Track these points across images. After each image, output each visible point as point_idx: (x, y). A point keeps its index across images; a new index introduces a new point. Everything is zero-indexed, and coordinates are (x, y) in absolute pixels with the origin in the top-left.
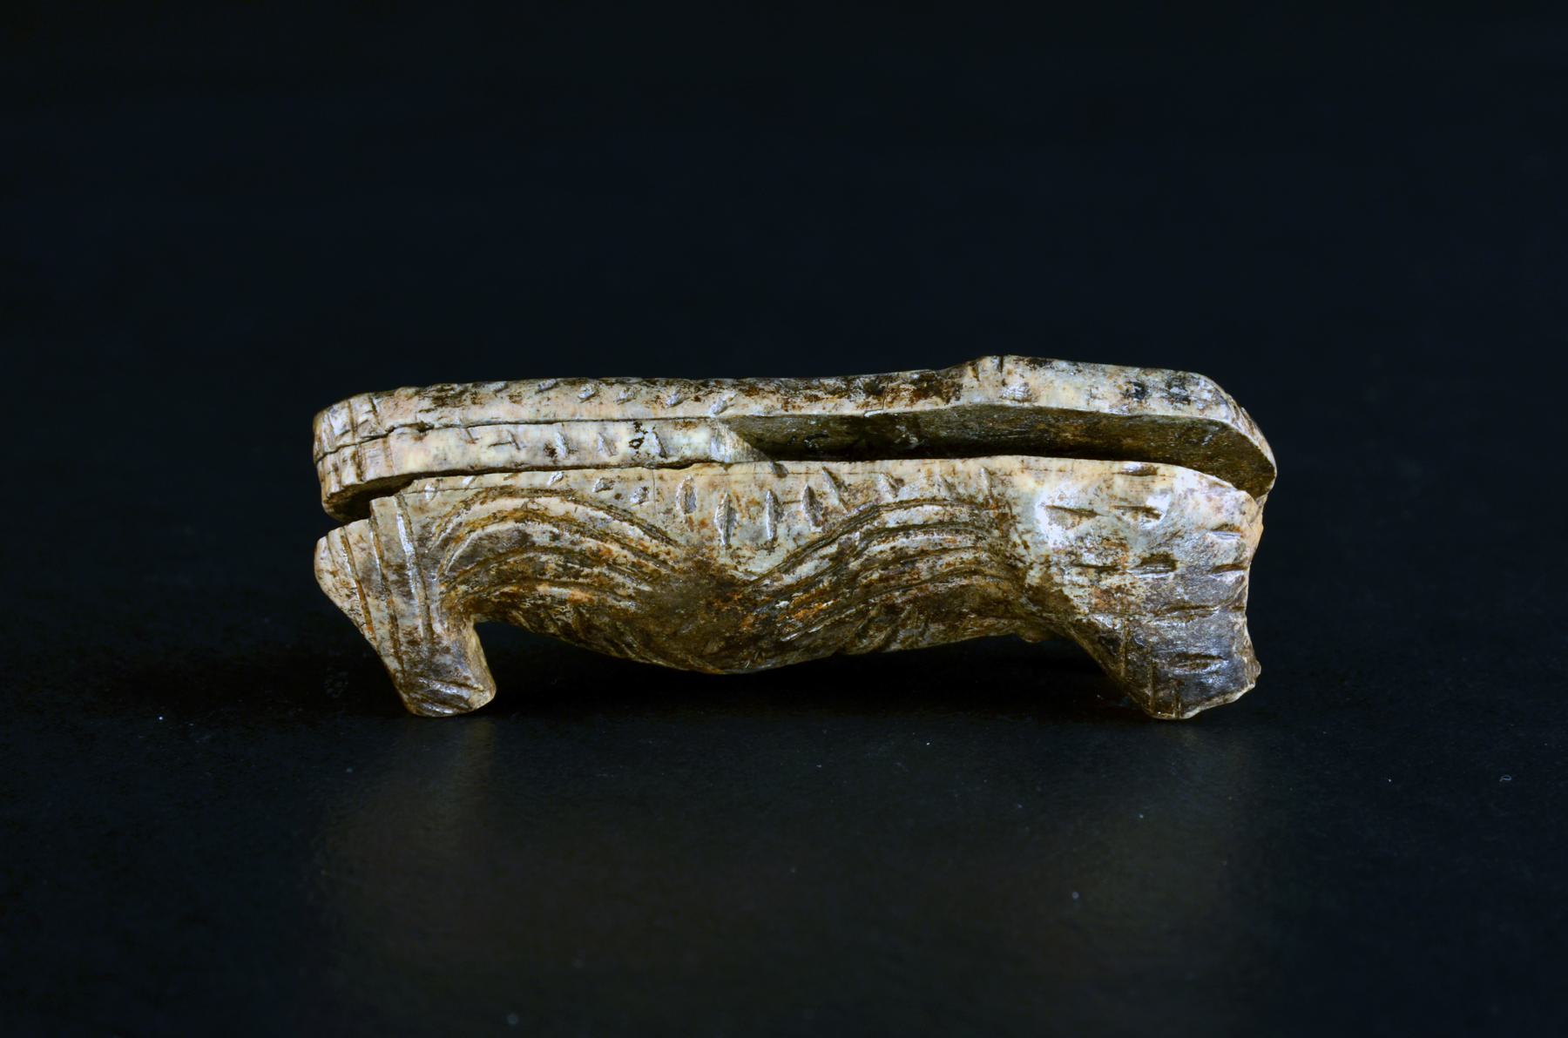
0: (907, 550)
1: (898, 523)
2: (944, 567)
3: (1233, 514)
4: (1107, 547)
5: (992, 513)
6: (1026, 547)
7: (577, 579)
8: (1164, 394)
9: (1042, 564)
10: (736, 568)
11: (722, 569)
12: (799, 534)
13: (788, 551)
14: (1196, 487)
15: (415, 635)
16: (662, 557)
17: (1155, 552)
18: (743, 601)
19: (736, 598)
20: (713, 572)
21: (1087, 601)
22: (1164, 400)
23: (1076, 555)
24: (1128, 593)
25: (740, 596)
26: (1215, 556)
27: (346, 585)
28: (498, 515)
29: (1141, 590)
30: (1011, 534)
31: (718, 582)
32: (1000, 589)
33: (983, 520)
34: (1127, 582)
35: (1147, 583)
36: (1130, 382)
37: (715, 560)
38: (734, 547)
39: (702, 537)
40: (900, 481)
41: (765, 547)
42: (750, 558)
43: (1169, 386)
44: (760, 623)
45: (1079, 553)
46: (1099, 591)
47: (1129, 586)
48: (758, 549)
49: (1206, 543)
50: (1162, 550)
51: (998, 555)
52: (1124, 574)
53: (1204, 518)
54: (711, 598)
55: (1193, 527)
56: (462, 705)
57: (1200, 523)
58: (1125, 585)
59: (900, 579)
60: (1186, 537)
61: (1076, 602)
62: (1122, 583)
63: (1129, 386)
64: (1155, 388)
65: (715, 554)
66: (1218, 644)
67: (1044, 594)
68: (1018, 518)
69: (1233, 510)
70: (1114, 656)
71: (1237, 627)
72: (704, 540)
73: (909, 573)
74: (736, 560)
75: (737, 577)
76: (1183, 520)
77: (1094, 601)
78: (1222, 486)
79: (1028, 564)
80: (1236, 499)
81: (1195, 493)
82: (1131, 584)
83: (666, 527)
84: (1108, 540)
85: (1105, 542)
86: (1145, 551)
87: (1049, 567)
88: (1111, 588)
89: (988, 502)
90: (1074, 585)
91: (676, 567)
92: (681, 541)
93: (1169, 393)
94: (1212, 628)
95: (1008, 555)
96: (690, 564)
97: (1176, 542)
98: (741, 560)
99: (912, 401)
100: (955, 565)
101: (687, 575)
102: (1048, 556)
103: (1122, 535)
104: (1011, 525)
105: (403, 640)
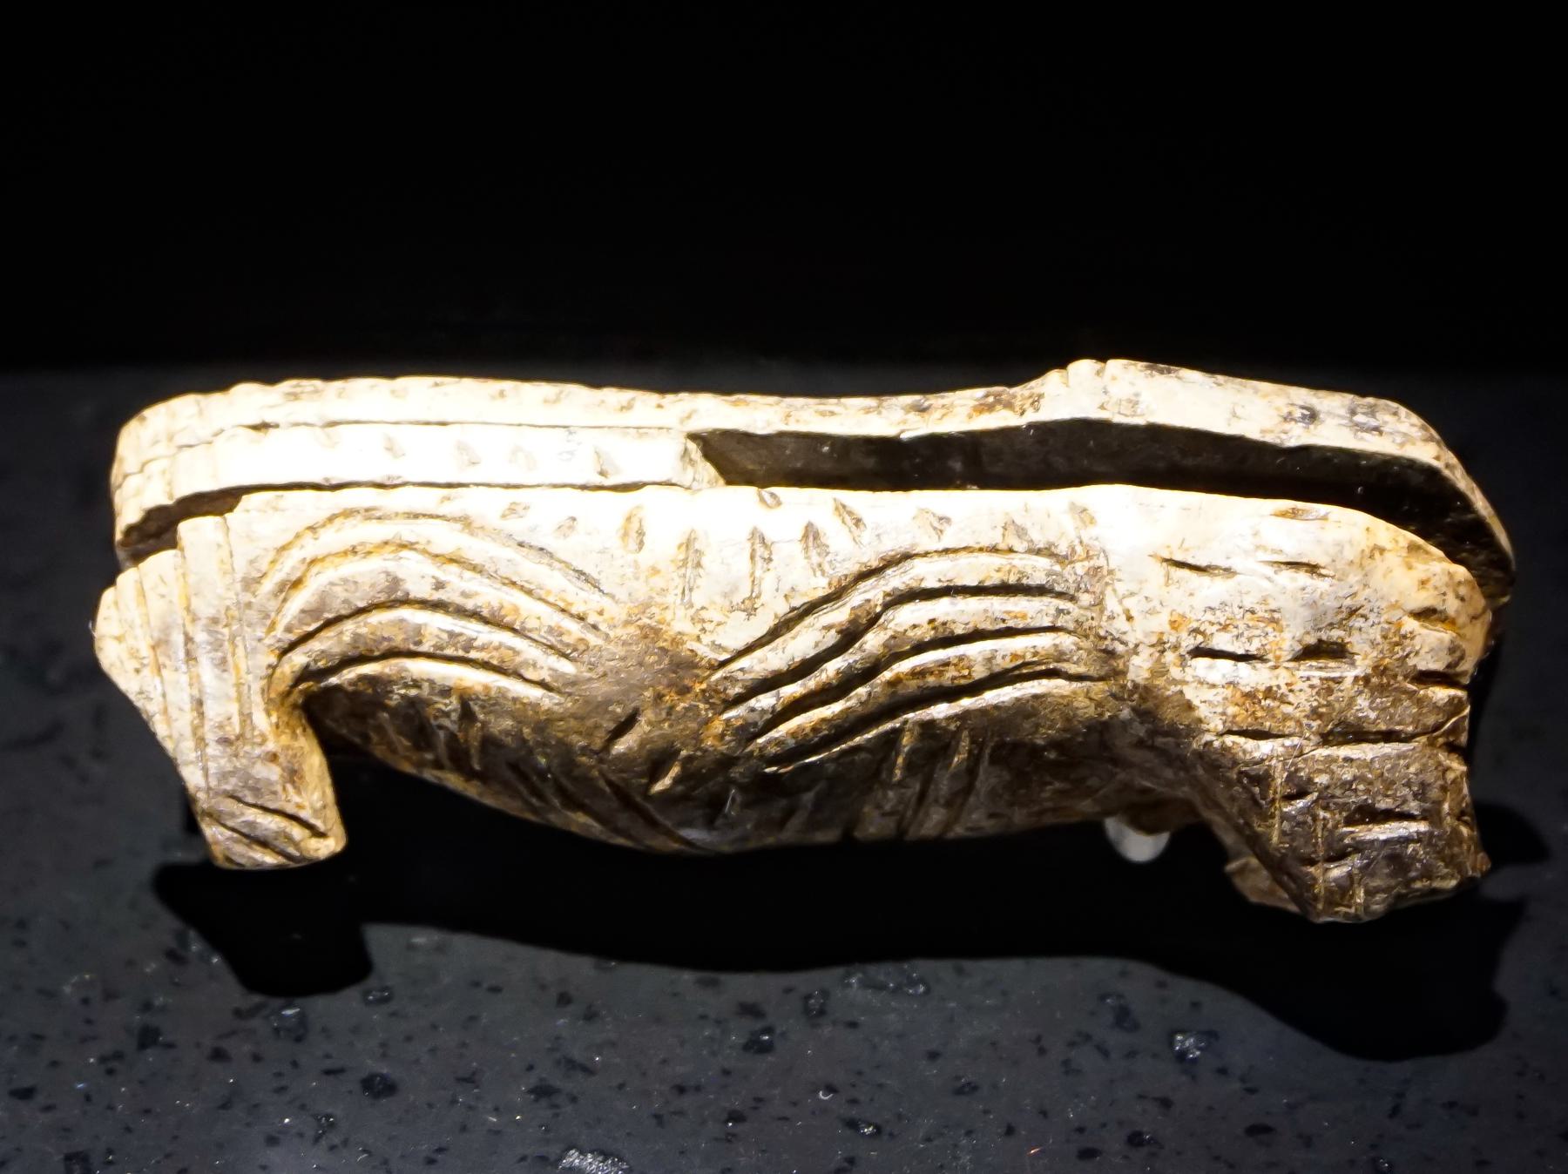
0: (953, 626)
1: (940, 581)
2: (1008, 659)
3: (1444, 594)
4: (1251, 624)
5: (1080, 568)
6: (1130, 618)
7: (468, 652)
8: (1344, 422)
9: (1153, 646)
10: (698, 639)
11: (677, 641)
12: (793, 589)
13: (776, 616)
14: (1388, 546)
15: (228, 728)
16: (591, 619)
17: (1324, 638)
18: (707, 694)
19: (698, 688)
20: (664, 644)
21: (1220, 710)
22: (1344, 428)
23: (1203, 633)
24: (1283, 700)
25: (704, 686)
26: (1417, 653)
27: (134, 654)
28: (358, 548)
29: (1303, 696)
30: (1107, 598)
31: (671, 661)
32: (1091, 699)
33: (1067, 581)
34: (1282, 683)
35: (1312, 687)
36: (1292, 405)
37: (669, 625)
38: (698, 606)
39: (651, 589)
40: (944, 519)
41: (743, 607)
42: (719, 624)
43: (1353, 413)
44: (732, 734)
45: (1208, 632)
46: (1238, 694)
47: (1284, 689)
48: (732, 609)
49: (1403, 632)
50: (1336, 634)
51: (1087, 637)
52: (1276, 667)
53: (1401, 593)
54: (660, 688)
55: (1384, 605)
56: (291, 850)
57: (1393, 600)
58: (1278, 687)
59: (941, 673)
60: (1372, 618)
61: (1203, 711)
62: (1274, 683)
63: (1291, 408)
64: (1329, 413)
65: (668, 615)
66: (1420, 795)
67: (1156, 698)
68: (1118, 575)
69: (1444, 589)
70: (1260, 806)
71: (1450, 776)
72: (654, 595)
73: (955, 665)
74: (699, 626)
75: (699, 653)
76: (1367, 591)
77: (1232, 710)
78: (1427, 552)
79: (1131, 646)
80: (1449, 573)
81: (1387, 554)
82: (1287, 684)
83: (599, 573)
84: (1253, 612)
85: (1248, 615)
86: (1308, 633)
87: (1162, 652)
88: (1258, 691)
89: (1073, 551)
90: (1201, 683)
91: (612, 634)
92: (621, 594)
93: (1351, 421)
94: (1412, 769)
95: (1102, 633)
96: (632, 630)
97: (1357, 625)
98: (706, 625)
99: (970, 417)
100: (1024, 657)
101: (628, 648)
102: (1162, 633)
103: (1273, 606)
104: (1107, 584)
105: (211, 737)
